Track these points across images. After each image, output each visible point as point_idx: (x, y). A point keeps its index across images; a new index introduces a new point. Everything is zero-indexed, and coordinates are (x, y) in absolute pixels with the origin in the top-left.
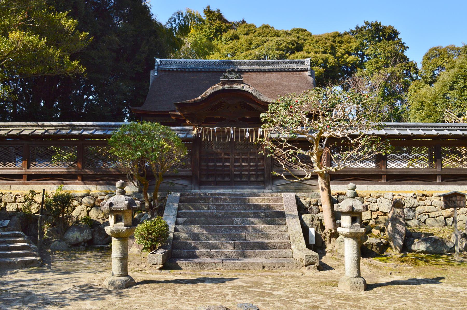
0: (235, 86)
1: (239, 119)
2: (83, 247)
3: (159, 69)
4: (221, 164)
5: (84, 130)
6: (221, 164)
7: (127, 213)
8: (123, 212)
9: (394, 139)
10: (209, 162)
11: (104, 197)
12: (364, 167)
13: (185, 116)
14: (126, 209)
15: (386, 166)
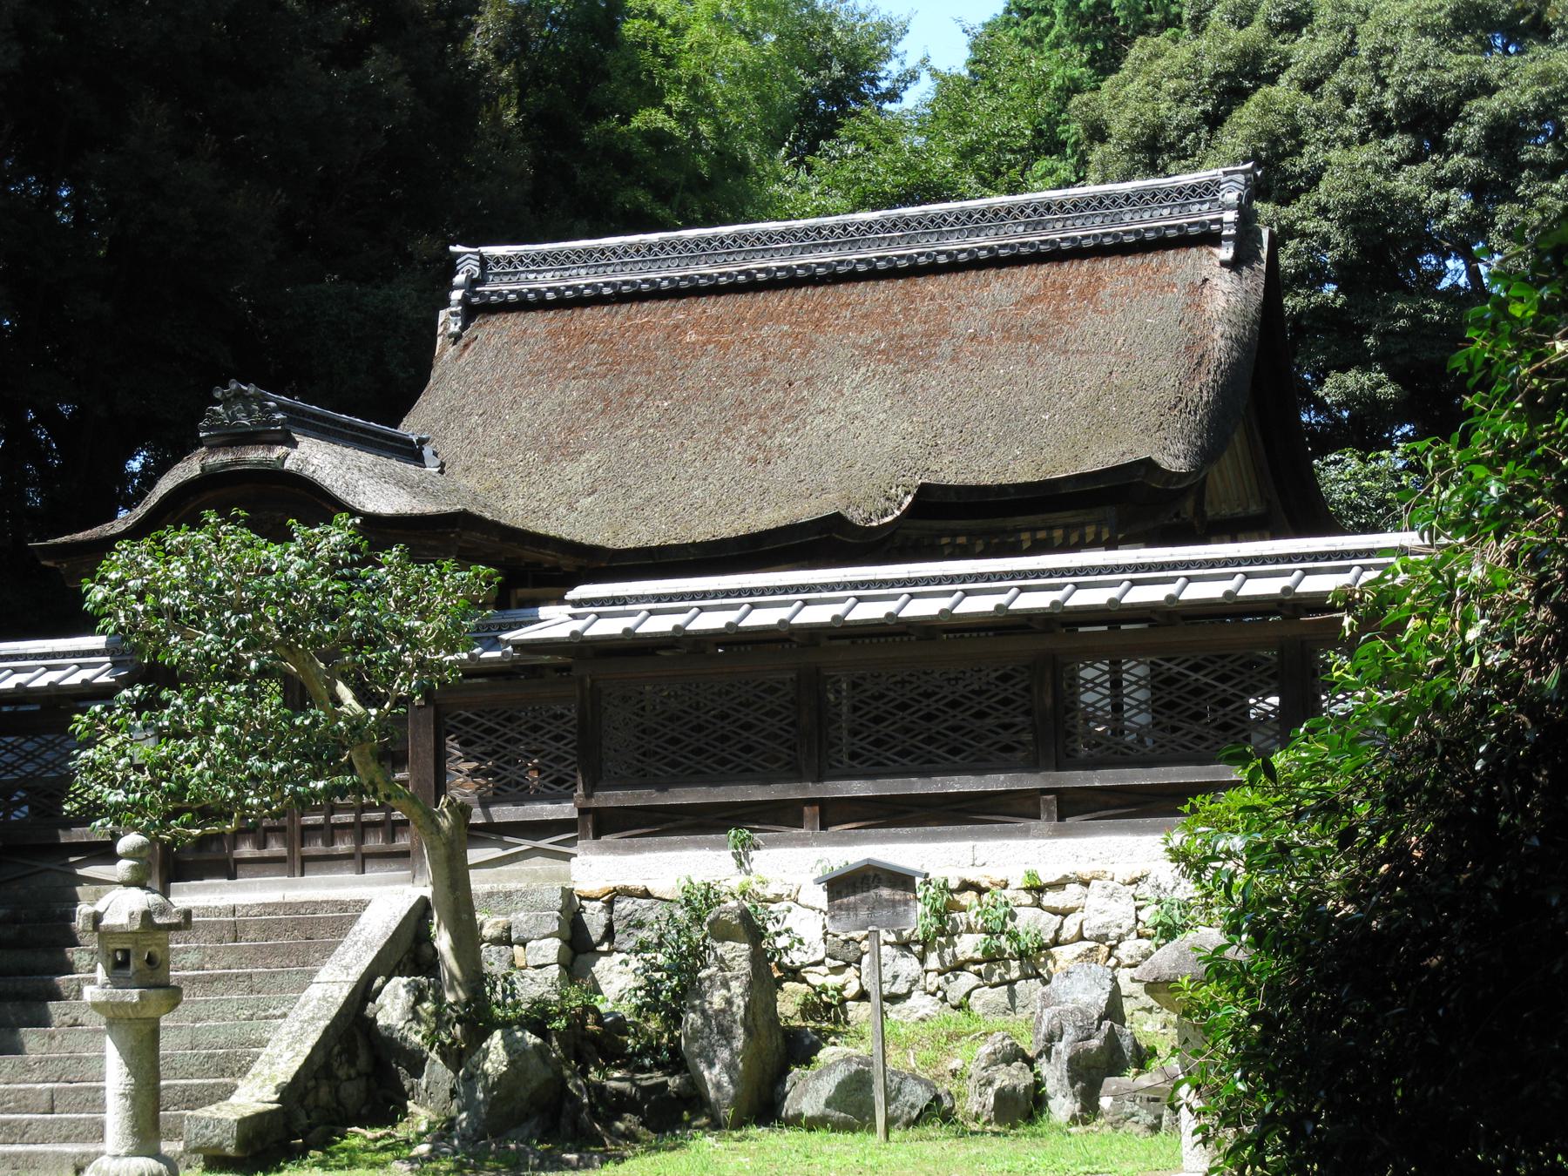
3: (475, 300)
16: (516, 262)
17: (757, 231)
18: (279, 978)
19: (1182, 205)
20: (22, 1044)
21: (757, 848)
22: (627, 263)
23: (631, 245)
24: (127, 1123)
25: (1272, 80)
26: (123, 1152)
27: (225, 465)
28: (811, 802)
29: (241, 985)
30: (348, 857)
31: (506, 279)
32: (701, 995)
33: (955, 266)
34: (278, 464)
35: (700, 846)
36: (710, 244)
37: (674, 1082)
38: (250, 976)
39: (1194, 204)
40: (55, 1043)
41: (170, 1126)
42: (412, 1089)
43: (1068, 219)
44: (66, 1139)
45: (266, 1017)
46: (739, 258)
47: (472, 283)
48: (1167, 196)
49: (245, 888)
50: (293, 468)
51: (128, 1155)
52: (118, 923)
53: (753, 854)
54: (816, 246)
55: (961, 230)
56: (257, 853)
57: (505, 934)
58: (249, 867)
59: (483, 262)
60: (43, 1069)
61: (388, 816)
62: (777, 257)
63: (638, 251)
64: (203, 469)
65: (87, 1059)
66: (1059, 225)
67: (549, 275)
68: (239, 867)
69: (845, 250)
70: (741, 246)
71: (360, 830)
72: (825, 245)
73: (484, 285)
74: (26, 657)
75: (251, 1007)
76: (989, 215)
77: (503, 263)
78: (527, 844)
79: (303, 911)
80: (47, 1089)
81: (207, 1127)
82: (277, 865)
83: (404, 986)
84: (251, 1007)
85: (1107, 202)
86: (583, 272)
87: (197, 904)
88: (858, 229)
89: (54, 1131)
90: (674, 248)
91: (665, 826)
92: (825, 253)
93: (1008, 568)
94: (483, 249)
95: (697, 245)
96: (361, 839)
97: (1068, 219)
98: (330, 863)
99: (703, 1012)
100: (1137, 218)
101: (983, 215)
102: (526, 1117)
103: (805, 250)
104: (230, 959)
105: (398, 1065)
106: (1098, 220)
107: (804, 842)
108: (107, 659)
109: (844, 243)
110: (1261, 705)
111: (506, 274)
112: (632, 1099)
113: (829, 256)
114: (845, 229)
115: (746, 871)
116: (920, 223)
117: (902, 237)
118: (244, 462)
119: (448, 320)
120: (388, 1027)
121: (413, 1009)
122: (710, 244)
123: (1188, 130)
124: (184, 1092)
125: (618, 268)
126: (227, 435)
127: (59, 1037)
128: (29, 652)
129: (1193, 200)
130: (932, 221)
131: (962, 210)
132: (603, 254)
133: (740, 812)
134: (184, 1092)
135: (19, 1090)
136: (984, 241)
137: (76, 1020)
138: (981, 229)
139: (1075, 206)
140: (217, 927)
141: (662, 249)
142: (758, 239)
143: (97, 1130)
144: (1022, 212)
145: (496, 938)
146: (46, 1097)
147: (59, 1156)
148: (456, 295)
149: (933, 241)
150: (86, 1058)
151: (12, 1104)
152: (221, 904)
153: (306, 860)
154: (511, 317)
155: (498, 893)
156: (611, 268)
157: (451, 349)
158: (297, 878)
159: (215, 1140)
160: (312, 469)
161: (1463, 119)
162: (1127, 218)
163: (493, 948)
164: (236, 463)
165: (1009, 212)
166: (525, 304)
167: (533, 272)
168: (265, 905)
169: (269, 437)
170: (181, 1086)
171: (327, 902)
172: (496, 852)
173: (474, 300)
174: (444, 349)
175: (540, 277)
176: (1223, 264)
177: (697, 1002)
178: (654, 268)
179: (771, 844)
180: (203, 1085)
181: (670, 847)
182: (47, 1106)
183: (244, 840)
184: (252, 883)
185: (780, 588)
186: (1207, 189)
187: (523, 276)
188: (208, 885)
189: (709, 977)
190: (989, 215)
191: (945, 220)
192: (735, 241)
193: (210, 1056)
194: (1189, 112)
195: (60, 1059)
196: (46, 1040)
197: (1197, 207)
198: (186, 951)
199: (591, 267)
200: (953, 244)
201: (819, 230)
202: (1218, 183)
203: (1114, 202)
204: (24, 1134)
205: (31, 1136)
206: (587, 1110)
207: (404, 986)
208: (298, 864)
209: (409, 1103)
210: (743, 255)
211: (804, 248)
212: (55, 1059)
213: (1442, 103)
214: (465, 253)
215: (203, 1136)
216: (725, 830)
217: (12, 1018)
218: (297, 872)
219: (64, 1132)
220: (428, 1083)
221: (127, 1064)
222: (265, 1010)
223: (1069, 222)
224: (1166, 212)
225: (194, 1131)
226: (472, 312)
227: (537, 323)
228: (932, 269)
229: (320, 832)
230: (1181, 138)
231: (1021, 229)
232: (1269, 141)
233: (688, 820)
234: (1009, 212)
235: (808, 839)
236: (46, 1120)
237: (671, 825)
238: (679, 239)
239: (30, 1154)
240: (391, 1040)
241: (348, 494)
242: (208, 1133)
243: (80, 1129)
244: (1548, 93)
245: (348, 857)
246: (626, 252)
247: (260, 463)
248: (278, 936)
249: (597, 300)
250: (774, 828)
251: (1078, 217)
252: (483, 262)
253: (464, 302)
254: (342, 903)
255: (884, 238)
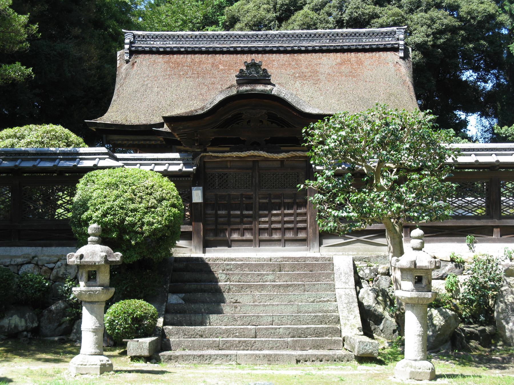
0: (260, 88)
1: (266, 140)
2: (25, 339)
3: (133, 49)
4: (238, 212)
5: (23, 160)
6: (238, 212)
7: (103, 269)
8: (99, 267)
9: (64, 157)
10: (219, 210)
11: (54, 265)
12: (464, 214)
13: (179, 137)
14: (103, 263)
15: (501, 213)
16: (146, 37)
17: (235, 34)
18: (317, 286)
19: (383, 38)
20: (222, 310)
21: (476, 243)
22: (187, 41)
23: (189, 35)
24: (420, 347)
25: (301, 8)
26: (419, 358)
27: (247, 91)
28: (497, 227)
29: (300, 289)
30: (279, 240)
31: (142, 43)
32: (503, 296)
33: (307, 51)
34: (270, 92)
35: (452, 241)
36: (218, 37)
37: (488, 329)
38: (304, 285)
39: (386, 38)
40: (237, 310)
41: (318, 344)
42: (375, 329)
43: (344, 39)
44: (272, 348)
45: (320, 301)
46: (229, 42)
47: (131, 43)
48: (378, 34)
49: (235, 251)
50: (276, 94)
51: (421, 360)
52: (424, 265)
53: (475, 245)
54: (256, 41)
55: (307, 40)
56: (240, 238)
57: (387, 272)
58: (237, 243)
59: (134, 36)
60: (241, 320)
61: (295, 226)
62: (242, 43)
63: (191, 37)
64: (238, 92)
65: (261, 316)
66: (341, 41)
67: (158, 43)
68: (232, 243)
69: (267, 42)
70: (229, 39)
71: (283, 231)
72: (259, 41)
73: (134, 44)
74: (145, 159)
75: (314, 297)
76: (317, 35)
77: (141, 37)
78: (355, 239)
79: (300, 260)
80: (254, 328)
81: (367, 346)
82: (249, 243)
83: (370, 290)
84: (314, 297)
85: (357, 35)
86: (171, 42)
87: (238, 257)
88: (271, 36)
89: (266, 345)
90: (205, 37)
91: (438, 233)
92: (259, 43)
93: (495, 147)
94: (133, 32)
95: (213, 37)
96: (284, 234)
97: (344, 39)
98: (271, 243)
99: (505, 303)
100: (367, 41)
101: (315, 35)
102: (446, 341)
103: (252, 42)
104: (287, 278)
105: (370, 320)
106: (354, 40)
107: (494, 241)
108: (181, 162)
109: (266, 40)
110: (463, 200)
111: (143, 41)
112: (476, 335)
113: (262, 44)
114: (266, 36)
115: (472, 251)
116: (293, 36)
117: (286, 40)
118: (255, 90)
119: (122, 55)
120: (369, 306)
121: (376, 299)
122: (218, 37)
123: (272, 21)
124: (314, 330)
125: (184, 42)
126: (247, 79)
127: (239, 307)
128: (147, 158)
129: (386, 36)
130: (297, 36)
131: (308, 33)
132: (178, 37)
133: (467, 229)
134: (314, 330)
135: (241, 328)
136: (316, 44)
137: (237, 301)
138: (315, 40)
139: (347, 35)
140: (273, 265)
141: (200, 37)
142: (235, 37)
143: (286, 345)
144: (328, 35)
145: (384, 273)
146: (253, 331)
147: (289, 356)
148: (127, 47)
149: (297, 42)
150: (260, 316)
151: (237, 334)
152: (265, 257)
153: (261, 241)
154: (147, 56)
155: (381, 256)
156: (182, 42)
157: (125, 66)
158: (257, 248)
159: (370, 351)
160: (283, 95)
161: (370, 25)
162: (364, 40)
163: (383, 276)
164: (252, 90)
165: (324, 35)
166: (151, 52)
167: (152, 41)
168: (284, 258)
169: (264, 82)
170: (313, 328)
171: (310, 257)
172: (342, 241)
173: (132, 49)
174: (121, 66)
175: (155, 43)
176: (401, 58)
177: (502, 299)
178: (198, 43)
179: (481, 241)
180: (323, 328)
181: (441, 241)
182: (254, 335)
183: (234, 233)
184: (240, 249)
185: (485, 149)
186: (391, 33)
187: (149, 42)
188: (218, 249)
189: (505, 290)
190: (317, 35)
191: (302, 36)
192: (227, 37)
193: (316, 316)
194: (272, 15)
195: (249, 316)
196: (233, 308)
197: (388, 39)
198: (268, 275)
199: (174, 41)
200: (305, 44)
201: (257, 36)
202: (395, 32)
203: (360, 35)
204: (252, 346)
205: (255, 347)
206: (464, 339)
207: (370, 290)
208: (257, 242)
209: (374, 335)
210: (230, 42)
211: (252, 41)
212: (247, 316)
213: (364, 19)
214: (128, 32)
215: (365, 349)
216: (465, 236)
217: (208, 299)
218: (257, 246)
219: (270, 346)
220: (384, 327)
221: (421, 323)
222: (319, 298)
223: (344, 40)
224: (377, 40)
225: (362, 347)
226: (132, 53)
227: (160, 59)
228: (300, 51)
229: (266, 231)
230: (269, 23)
231: (328, 41)
232: (307, 26)
233: (447, 232)
234: (324, 35)
235: (496, 240)
236: (262, 341)
237: (440, 233)
238: (207, 34)
239: (276, 355)
240: (369, 310)
241: (298, 105)
242: (367, 348)
243: (278, 344)
244: (397, 19)
245: (279, 240)
246: (187, 37)
247: (262, 91)
248: (298, 270)
249: (179, 52)
250: (481, 236)
251: (348, 39)
252: (134, 36)
253: (129, 49)
254: (316, 258)
255: (280, 40)
